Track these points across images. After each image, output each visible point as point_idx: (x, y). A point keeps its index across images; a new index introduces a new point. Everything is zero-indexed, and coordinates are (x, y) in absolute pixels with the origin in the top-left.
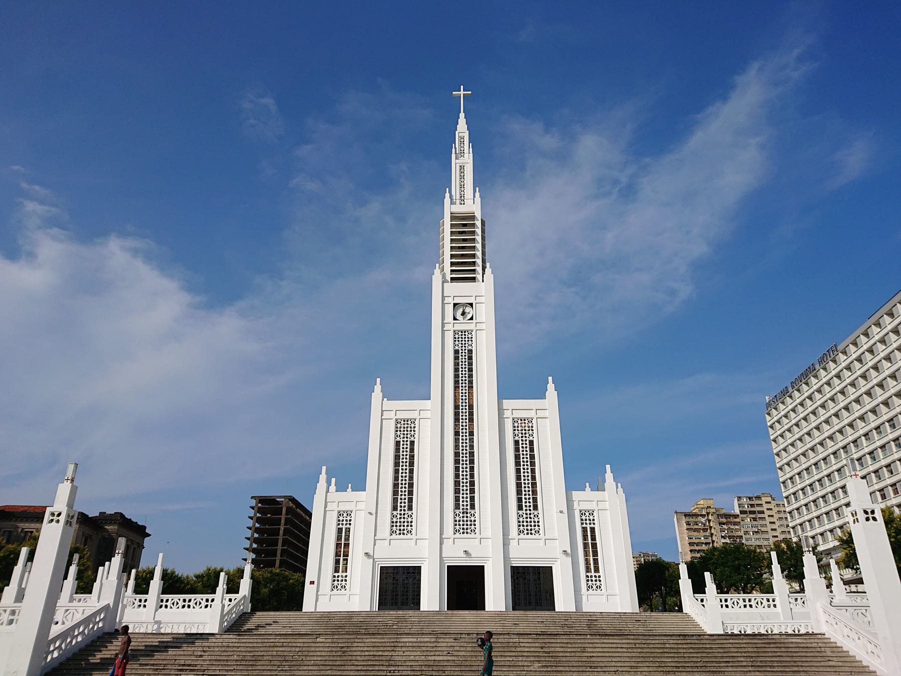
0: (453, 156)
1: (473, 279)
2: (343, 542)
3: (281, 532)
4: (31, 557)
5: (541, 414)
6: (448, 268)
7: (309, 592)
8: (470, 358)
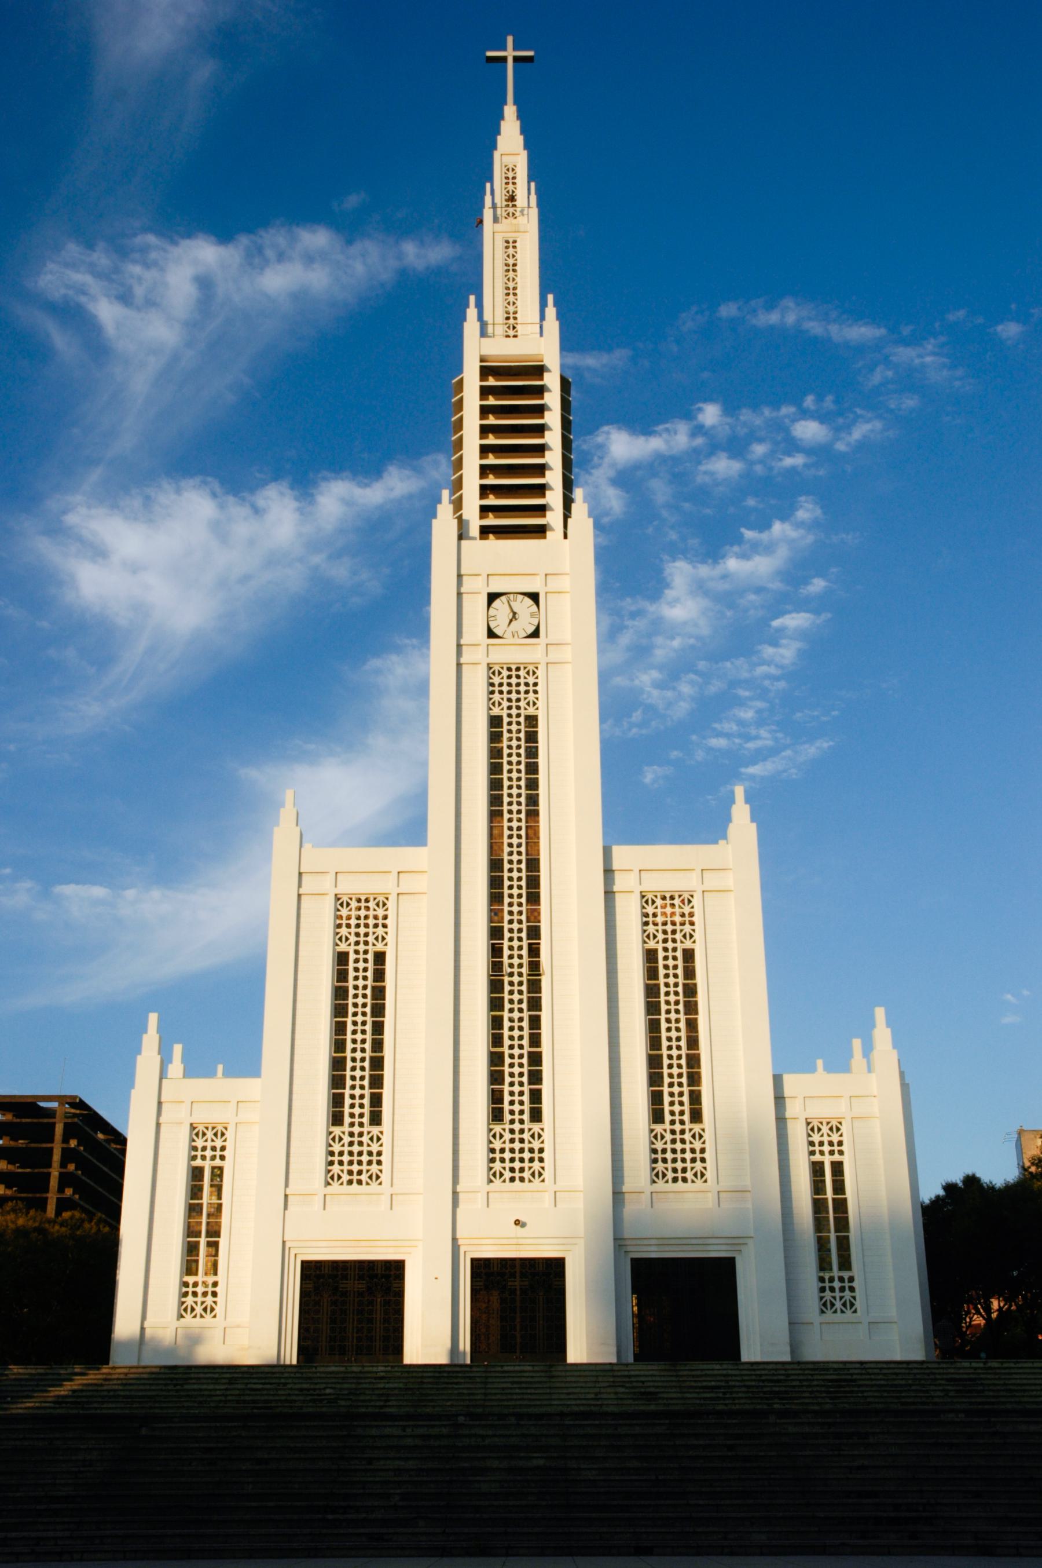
1: (540, 531)
4: (479, 305)
5: (712, 881)
8: (532, 737)
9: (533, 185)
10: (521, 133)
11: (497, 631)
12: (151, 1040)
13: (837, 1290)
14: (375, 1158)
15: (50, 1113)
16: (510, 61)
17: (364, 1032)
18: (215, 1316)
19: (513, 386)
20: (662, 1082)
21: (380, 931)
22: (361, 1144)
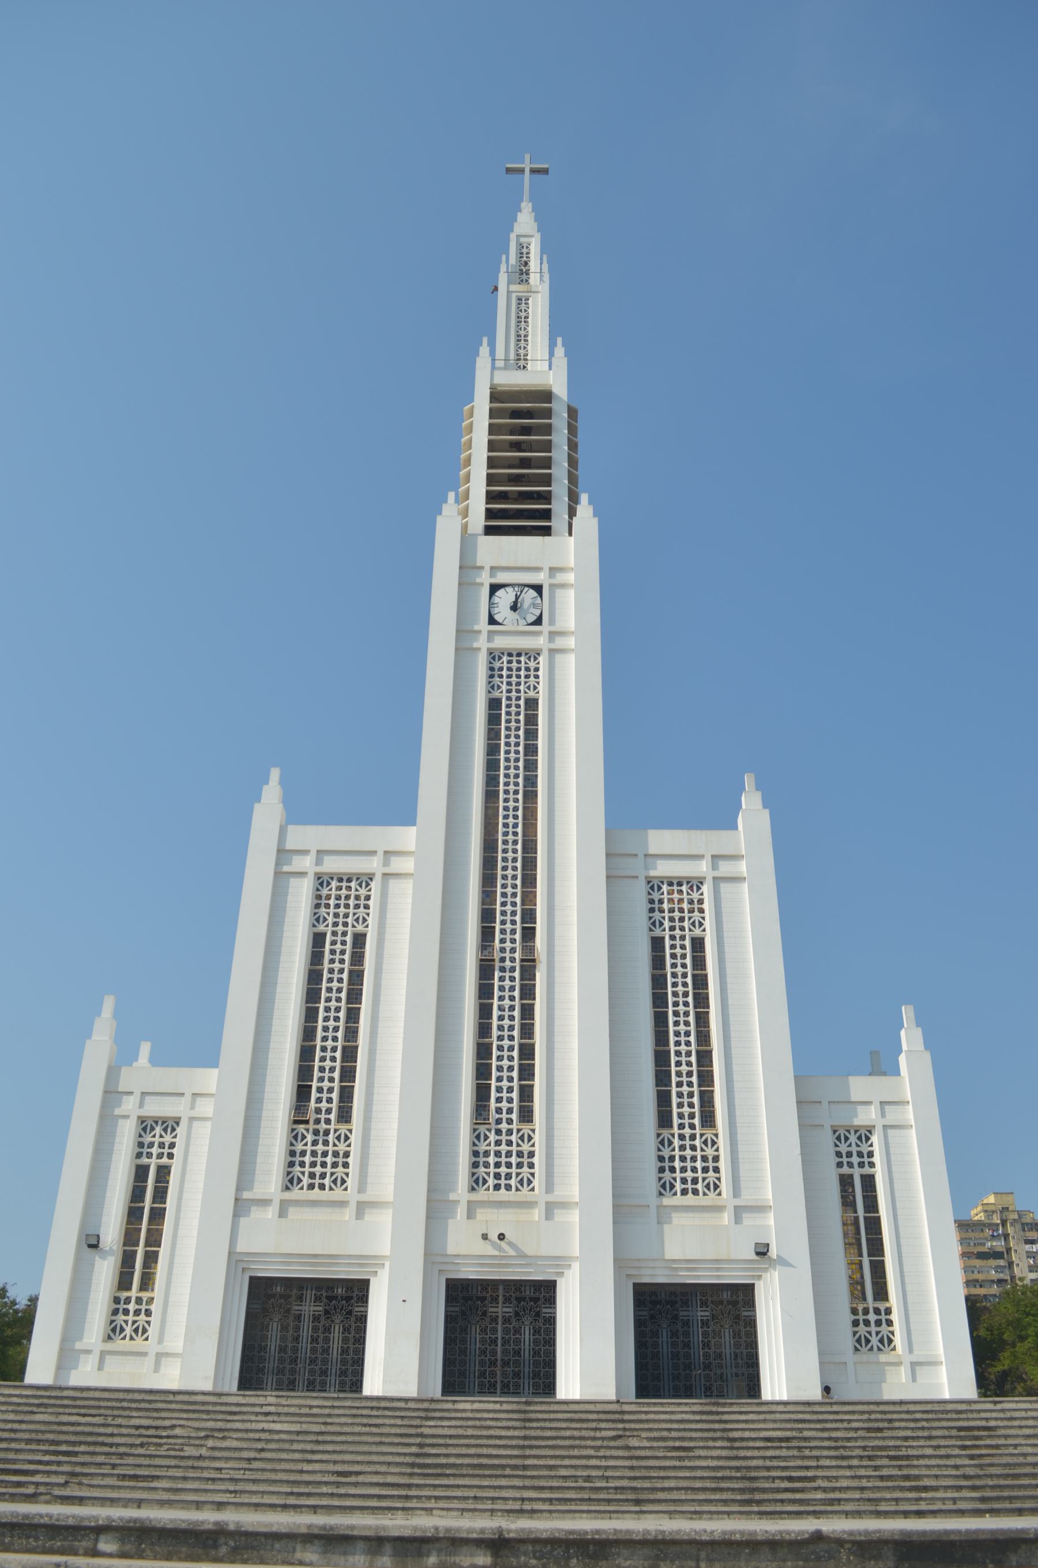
1: (546, 531)
5: (725, 868)
6: (478, 505)
9: (545, 257)
10: (535, 221)
11: (497, 617)
13: (873, 1324)
14: (341, 1160)
16: (527, 171)
17: (342, 961)
18: (147, 1339)
19: (521, 418)
20: (670, 1081)
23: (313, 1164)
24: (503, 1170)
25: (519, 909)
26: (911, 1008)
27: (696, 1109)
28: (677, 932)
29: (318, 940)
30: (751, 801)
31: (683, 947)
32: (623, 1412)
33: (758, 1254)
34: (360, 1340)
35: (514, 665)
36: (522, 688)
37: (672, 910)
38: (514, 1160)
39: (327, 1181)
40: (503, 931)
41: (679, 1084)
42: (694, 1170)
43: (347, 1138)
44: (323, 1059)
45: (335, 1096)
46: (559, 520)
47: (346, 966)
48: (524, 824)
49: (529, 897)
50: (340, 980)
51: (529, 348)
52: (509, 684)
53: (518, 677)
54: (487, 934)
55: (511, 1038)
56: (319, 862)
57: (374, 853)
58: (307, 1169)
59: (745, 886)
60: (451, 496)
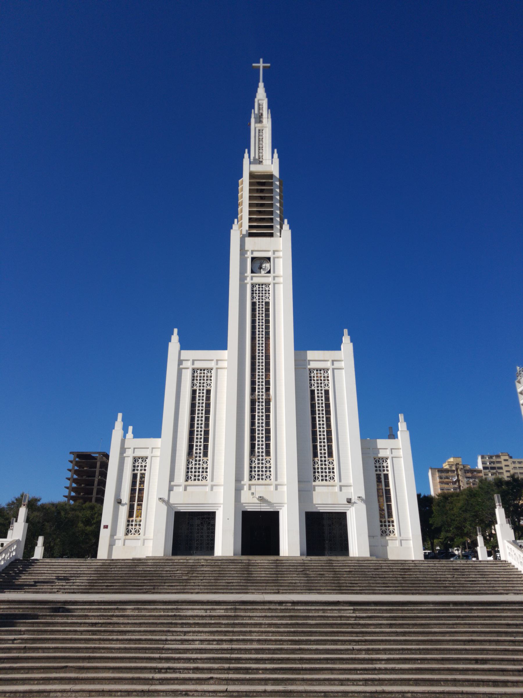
0: (253, 120)
1: (271, 235)
2: (137, 488)
3: (96, 483)
4: (249, 153)
7: (104, 535)
9: (269, 110)
12: (119, 424)
14: (205, 470)
15: (94, 458)
19: (261, 182)
21: (209, 382)
22: (199, 464)
23: (195, 472)
24: (260, 473)
25: (264, 380)
26: (402, 415)
27: (326, 451)
28: (320, 388)
29: (194, 392)
30: (346, 340)
31: (322, 393)
32: (304, 563)
33: (348, 502)
34: (213, 532)
35: (261, 289)
36: (264, 298)
37: (317, 380)
38: (264, 469)
39: (200, 478)
40: (259, 389)
41: (320, 442)
42: (326, 472)
43: (207, 462)
44: (197, 435)
45: (202, 448)
46: (276, 230)
47: (204, 401)
48: (265, 349)
49: (267, 376)
50: (202, 407)
51: (264, 153)
52: (259, 296)
53: (262, 293)
54: (253, 390)
55: (262, 427)
56: (193, 364)
57: (212, 360)
58: (193, 474)
59: (344, 371)
60: (236, 220)
